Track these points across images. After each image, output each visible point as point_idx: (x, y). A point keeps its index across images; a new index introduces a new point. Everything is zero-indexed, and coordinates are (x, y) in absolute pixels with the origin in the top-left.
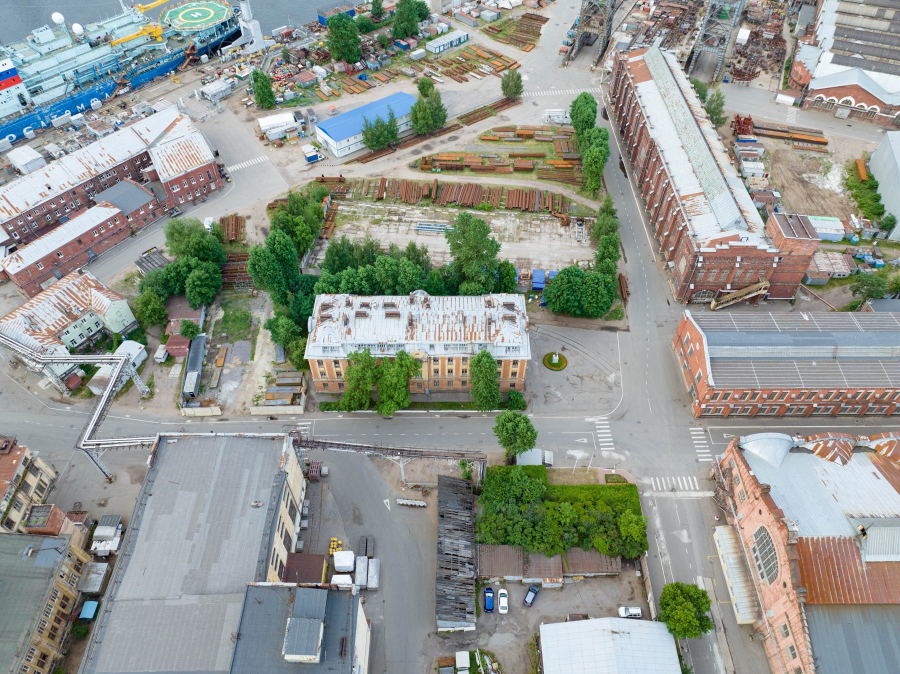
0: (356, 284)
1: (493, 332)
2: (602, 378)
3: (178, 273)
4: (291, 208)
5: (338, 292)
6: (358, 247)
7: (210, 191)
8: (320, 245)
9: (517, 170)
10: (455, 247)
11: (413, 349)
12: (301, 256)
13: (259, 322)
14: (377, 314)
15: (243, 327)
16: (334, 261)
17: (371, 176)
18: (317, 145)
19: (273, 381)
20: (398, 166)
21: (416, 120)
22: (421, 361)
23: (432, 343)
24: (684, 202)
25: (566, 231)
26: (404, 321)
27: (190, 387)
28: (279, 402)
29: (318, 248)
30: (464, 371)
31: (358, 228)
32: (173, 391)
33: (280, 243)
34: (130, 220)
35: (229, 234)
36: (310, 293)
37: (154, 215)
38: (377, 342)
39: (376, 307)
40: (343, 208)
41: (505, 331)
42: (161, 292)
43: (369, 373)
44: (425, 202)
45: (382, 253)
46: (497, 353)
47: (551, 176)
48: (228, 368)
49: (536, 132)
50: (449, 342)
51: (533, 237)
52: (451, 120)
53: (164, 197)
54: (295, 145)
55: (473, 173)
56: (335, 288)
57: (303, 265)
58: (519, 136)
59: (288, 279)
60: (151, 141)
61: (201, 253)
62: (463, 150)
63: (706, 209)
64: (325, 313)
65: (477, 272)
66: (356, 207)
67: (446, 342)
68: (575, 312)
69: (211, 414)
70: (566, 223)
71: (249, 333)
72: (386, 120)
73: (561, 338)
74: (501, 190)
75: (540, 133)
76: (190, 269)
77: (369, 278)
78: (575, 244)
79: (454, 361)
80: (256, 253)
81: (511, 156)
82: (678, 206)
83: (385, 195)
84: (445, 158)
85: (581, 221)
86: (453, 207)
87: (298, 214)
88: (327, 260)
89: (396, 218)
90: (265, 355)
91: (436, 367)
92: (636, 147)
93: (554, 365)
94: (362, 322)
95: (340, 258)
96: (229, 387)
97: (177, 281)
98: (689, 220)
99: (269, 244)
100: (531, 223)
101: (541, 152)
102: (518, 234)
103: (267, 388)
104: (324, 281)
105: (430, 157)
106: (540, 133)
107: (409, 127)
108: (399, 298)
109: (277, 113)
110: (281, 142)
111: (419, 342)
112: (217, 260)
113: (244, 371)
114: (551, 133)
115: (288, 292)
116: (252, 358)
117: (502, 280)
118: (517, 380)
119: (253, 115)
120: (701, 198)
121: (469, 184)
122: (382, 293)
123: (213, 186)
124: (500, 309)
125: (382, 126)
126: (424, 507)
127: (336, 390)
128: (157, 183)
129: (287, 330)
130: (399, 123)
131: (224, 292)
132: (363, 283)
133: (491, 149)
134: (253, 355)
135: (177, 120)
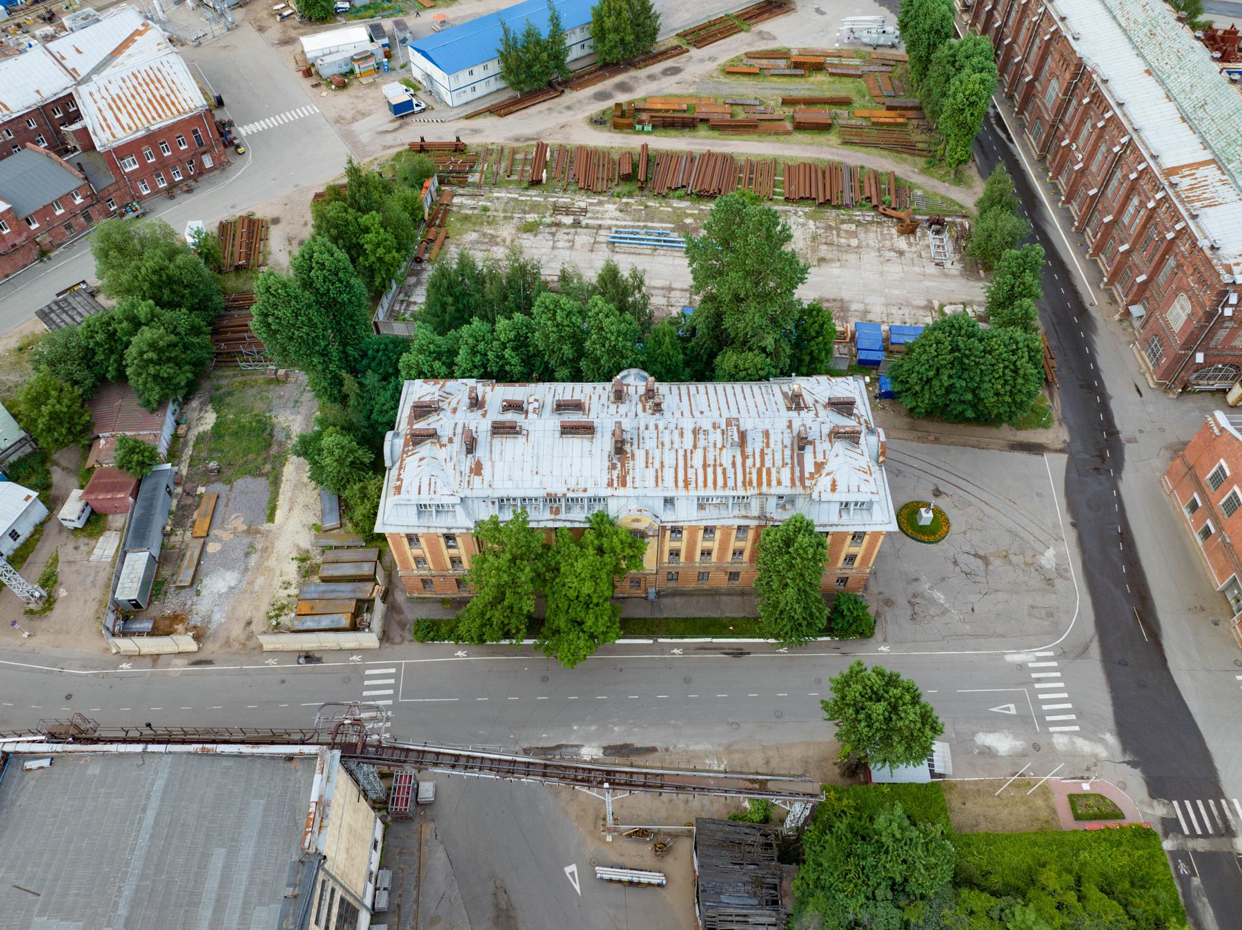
0: (491, 355)
1: (809, 468)
2: (1029, 560)
3: (112, 335)
4: (353, 197)
5: (451, 375)
6: (494, 277)
7: (201, 171)
8: (417, 273)
9: (800, 127)
10: (703, 276)
11: (625, 508)
12: (377, 296)
13: (288, 437)
14: (542, 426)
15: (253, 449)
16: (444, 306)
17: (517, 140)
18: (411, 84)
19: (313, 570)
20: (568, 121)
21: (600, 33)
22: (643, 535)
23: (669, 494)
24: (1175, 179)
25: (910, 245)
26: (604, 443)
27: (129, 589)
28: (325, 622)
29: (412, 280)
30: (738, 553)
31: (493, 240)
32: (96, 593)
33: (322, 266)
34: (34, 226)
35: (235, 253)
36: (391, 378)
37: (88, 218)
38: (542, 493)
39: (539, 411)
40: (462, 201)
41: (836, 469)
42: (77, 376)
43: (526, 574)
44: (625, 188)
45: (545, 286)
46: (825, 517)
47: (866, 140)
48: (218, 539)
49: (829, 60)
50: (709, 492)
51: (845, 257)
52: (665, 39)
53: (106, 180)
54: (370, 85)
55: (716, 134)
56: (444, 365)
57: (381, 314)
58: (797, 65)
59: (345, 345)
60: (83, 72)
61: (166, 292)
62: (691, 91)
63: (1228, 193)
64: (421, 425)
65: (747, 329)
66: (488, 199)
67: (702, 493)
68: (962, 412)
69: (175, 649)
70: (909, 229)
71: (265, 461)
72: (545, 33)
73: (926, 467)
74: (770, 166)
75: (836, 61)
76: (136, 324)
77: (520, 342)
78: (932, 269)
79: (718, 534)
80: (268, 289)
81: (786, 102)
82: (1158, 187)
83: (544, 175)
84: (659, 106)
85: (937, 224)
86: (680, 198)
87: (365, 211)
88: (430, 304)
89: (568, 220)
90: (298, 513)
91: (675, 545)
92: (1031, 84)
93: (923, 530)
94: (509, 445)
95: (457, 300)
96: (218, 583)
97: (112, 352)
98: (1194, 217)
99: (298, 269)
100: (838, 230)
101: (843, 94)
102: (814, 250)
103: (299, 586)
104: (421, 351)
105: (630, 103)
106: (836, 61)
107: (587, 51)
108: (588, 387)
109: (336, 28)
110: (343, 81)
111: (640, 492)
112: (201, 306)
113: (251, 546)
114: (857, 62)
115: (343, 373)
116: (271, 518)
117: (805, 346)
118: (853, 572)
119: (293, 33)
120: (1211, 172)
121: (710, 154)
122: (548, 376)
123: (208, 162)
124: (823, 413)
125: (538, 43)
126: (660, 885)
127: (452, 593)
128: (92, 155)
129: (340, 461)
130: (568, 42)
131: (220, 373)
132: (508, 353)
133: (746, 89)
134: (273, 509)
135: (137, 33)
